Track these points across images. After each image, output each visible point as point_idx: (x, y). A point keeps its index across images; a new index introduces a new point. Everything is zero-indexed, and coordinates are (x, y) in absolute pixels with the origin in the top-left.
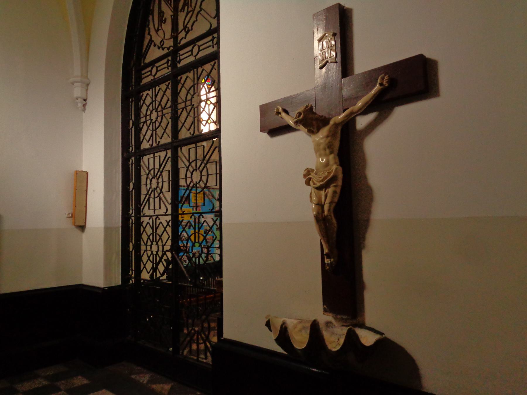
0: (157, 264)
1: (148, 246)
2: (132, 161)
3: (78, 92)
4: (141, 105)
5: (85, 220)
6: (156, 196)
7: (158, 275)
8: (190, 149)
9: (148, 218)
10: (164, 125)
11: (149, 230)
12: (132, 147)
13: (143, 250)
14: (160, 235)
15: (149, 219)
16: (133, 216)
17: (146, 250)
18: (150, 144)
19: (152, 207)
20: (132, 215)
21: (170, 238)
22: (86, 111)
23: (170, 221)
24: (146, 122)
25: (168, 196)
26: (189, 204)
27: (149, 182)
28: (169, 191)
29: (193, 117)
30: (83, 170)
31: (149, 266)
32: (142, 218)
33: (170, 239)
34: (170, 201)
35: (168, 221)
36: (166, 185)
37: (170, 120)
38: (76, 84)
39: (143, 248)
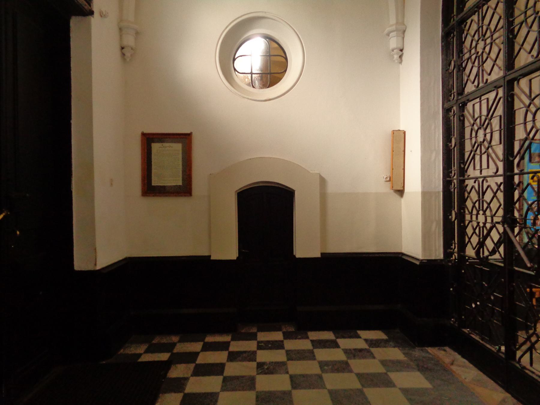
0: (485, 238)
1: (473, 216)
2: (454, 186)
3: (393, 43)
4: (465, 36)
5: (403, 184)
6: (483, 152)
7: (486, 253)
8: (532, 80)
9: (473, 180)
10: (493, 55)
11: (474, 196)
12: (455, 171)
13: (467, 220)
14: (489, 201)
15: (475, 182)
16: (455, 179)
17: (471, 221)
18: (475, 86)
19: (478, 167)
20: (454, 177)
21: (502, 207)
22: (403, 63)
23: (501, 183)
24: (470, 58)
25: (500, 150)
26: (523, 175)
27: (474, 134)
28: (501, 143)
29: (537, 31)
30: (400, 129)
31: (475, 240)
32: (466, 181)
33: (501, 208)
34: (501, 157)
35: (499, 183)
36: (496, 136)
37: (502, 46)
38: (391, 35)
39: (468, 217)
